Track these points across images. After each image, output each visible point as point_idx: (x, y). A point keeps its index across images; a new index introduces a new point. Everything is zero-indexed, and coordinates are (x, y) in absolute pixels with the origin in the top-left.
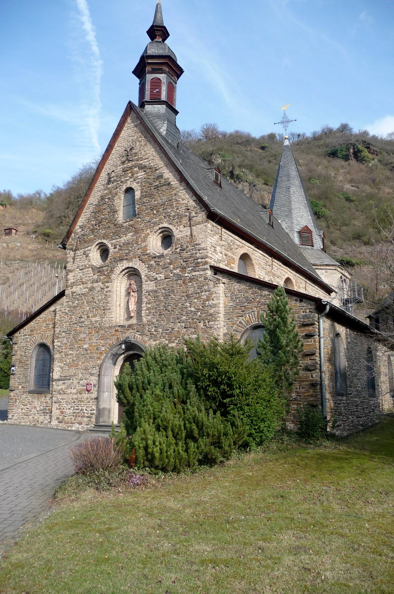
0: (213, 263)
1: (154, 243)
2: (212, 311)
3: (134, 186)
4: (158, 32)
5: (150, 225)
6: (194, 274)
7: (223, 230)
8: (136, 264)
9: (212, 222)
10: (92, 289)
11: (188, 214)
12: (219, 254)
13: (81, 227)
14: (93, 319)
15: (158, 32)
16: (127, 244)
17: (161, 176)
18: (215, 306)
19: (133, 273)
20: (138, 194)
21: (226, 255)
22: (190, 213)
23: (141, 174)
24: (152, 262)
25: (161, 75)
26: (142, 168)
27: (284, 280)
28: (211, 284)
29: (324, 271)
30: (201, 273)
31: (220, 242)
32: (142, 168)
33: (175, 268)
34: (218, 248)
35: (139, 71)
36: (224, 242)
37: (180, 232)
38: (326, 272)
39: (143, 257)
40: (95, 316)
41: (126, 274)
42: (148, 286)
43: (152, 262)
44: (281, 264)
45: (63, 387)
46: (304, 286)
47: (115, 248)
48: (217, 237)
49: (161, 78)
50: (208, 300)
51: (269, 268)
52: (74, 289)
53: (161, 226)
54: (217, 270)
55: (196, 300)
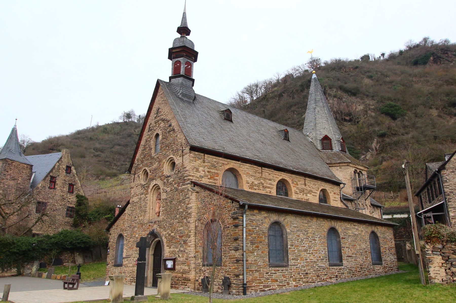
0: (194, 179)
1: (166, 169)
2: (189, 211)
3: (160, 132)
4: (184, 30)
5: (165, 156)
6: (183, 187)
7: (206, 155)
8: (159, 182)
9: (194, 152)
10: (140, 199)
11: (181, 148)
12: (202, 172)
13: (138, 160)
14: (140, 218)
15: (184, 30)
16: (155, 169)
17: (170, 126)
18: (191, 208)
19: (157, 188)
20: (160, 137)
21: (208, 172)
22: (182, 147)
23: (162, 125)
24: (165, 181)
25: (181, 58)
26: (163, 120)
27: (277, 181)
28: (190, 193)
29: (338, 168)
30: (186, 186)
31: (203, 164)
32: (163, 120)
33: (175, 183)
34: (201, 169)
35: (170, 58)
36: (206, 164)
37: (178, 161)
38: (340, 168)
39: (162, 177)
40: (141, 216)
41: (155, 189)
42: (164, 196)
43: (165, 181)
44: (273, 170)
45: (127, 262)
46: (303, 182)
47: (151, 172)
48: (199, 162)
49: (181, 60)
50: (188, 204)
51: (258, 175)
52: (133, 200)
53: (169, 157)
54: (195, 184)
55: (183, 205)
